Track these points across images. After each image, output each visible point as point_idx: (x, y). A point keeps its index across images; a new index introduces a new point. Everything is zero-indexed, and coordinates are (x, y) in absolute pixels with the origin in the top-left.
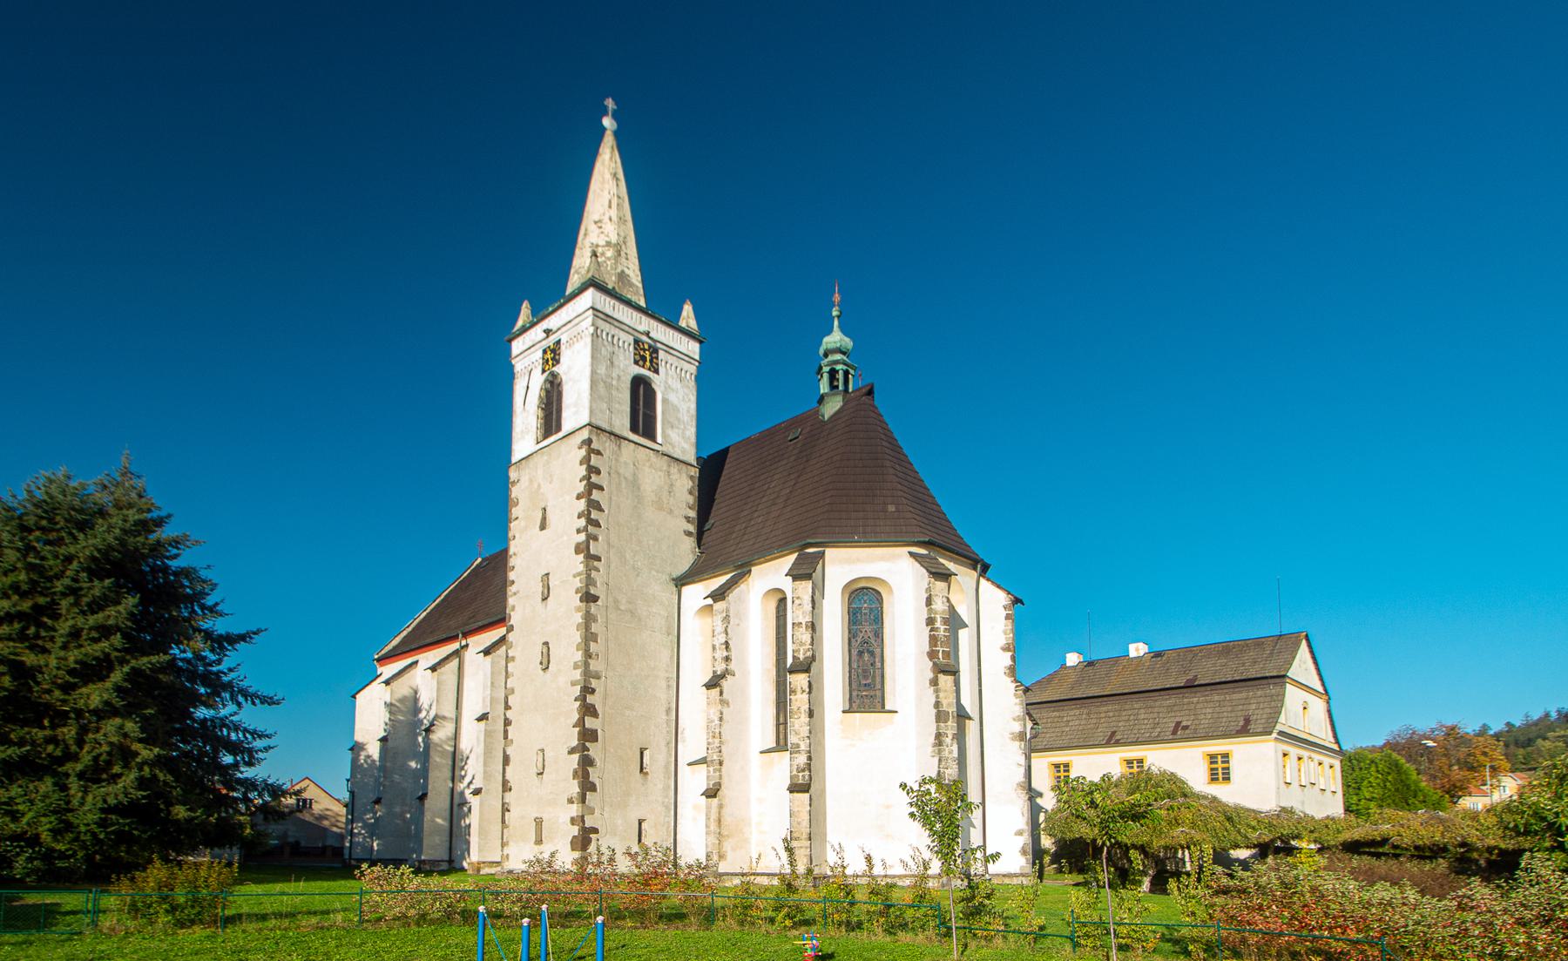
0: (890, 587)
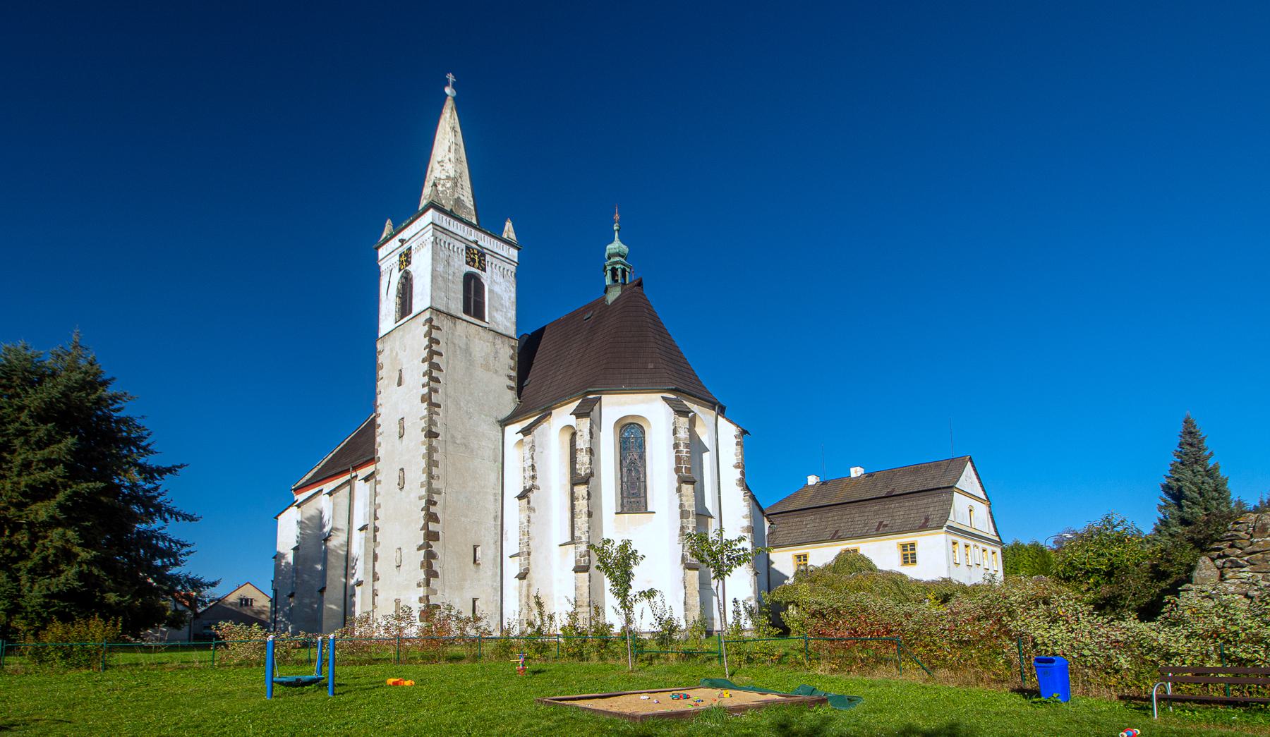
0: (650, 425)
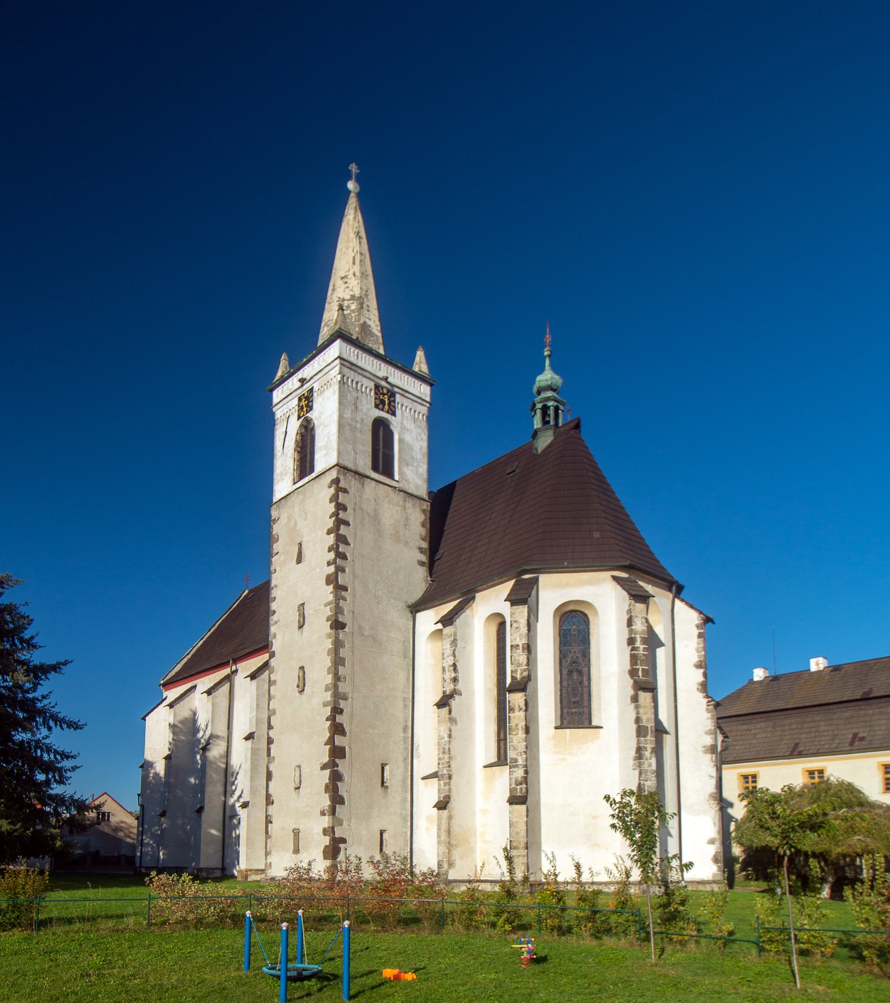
0: (595, 610)
